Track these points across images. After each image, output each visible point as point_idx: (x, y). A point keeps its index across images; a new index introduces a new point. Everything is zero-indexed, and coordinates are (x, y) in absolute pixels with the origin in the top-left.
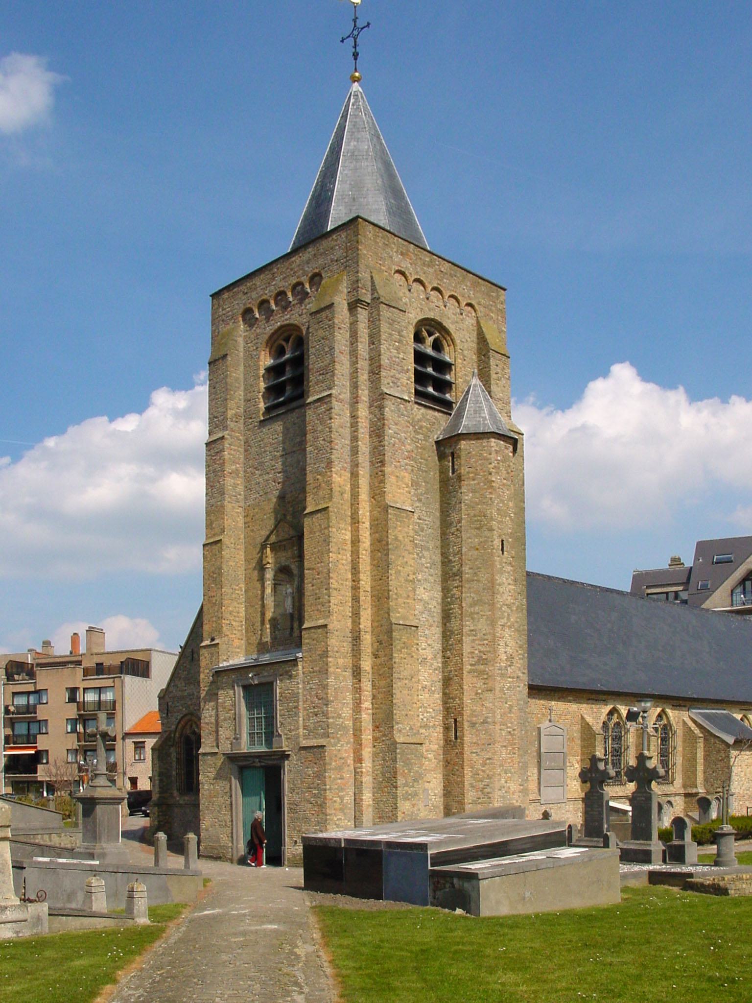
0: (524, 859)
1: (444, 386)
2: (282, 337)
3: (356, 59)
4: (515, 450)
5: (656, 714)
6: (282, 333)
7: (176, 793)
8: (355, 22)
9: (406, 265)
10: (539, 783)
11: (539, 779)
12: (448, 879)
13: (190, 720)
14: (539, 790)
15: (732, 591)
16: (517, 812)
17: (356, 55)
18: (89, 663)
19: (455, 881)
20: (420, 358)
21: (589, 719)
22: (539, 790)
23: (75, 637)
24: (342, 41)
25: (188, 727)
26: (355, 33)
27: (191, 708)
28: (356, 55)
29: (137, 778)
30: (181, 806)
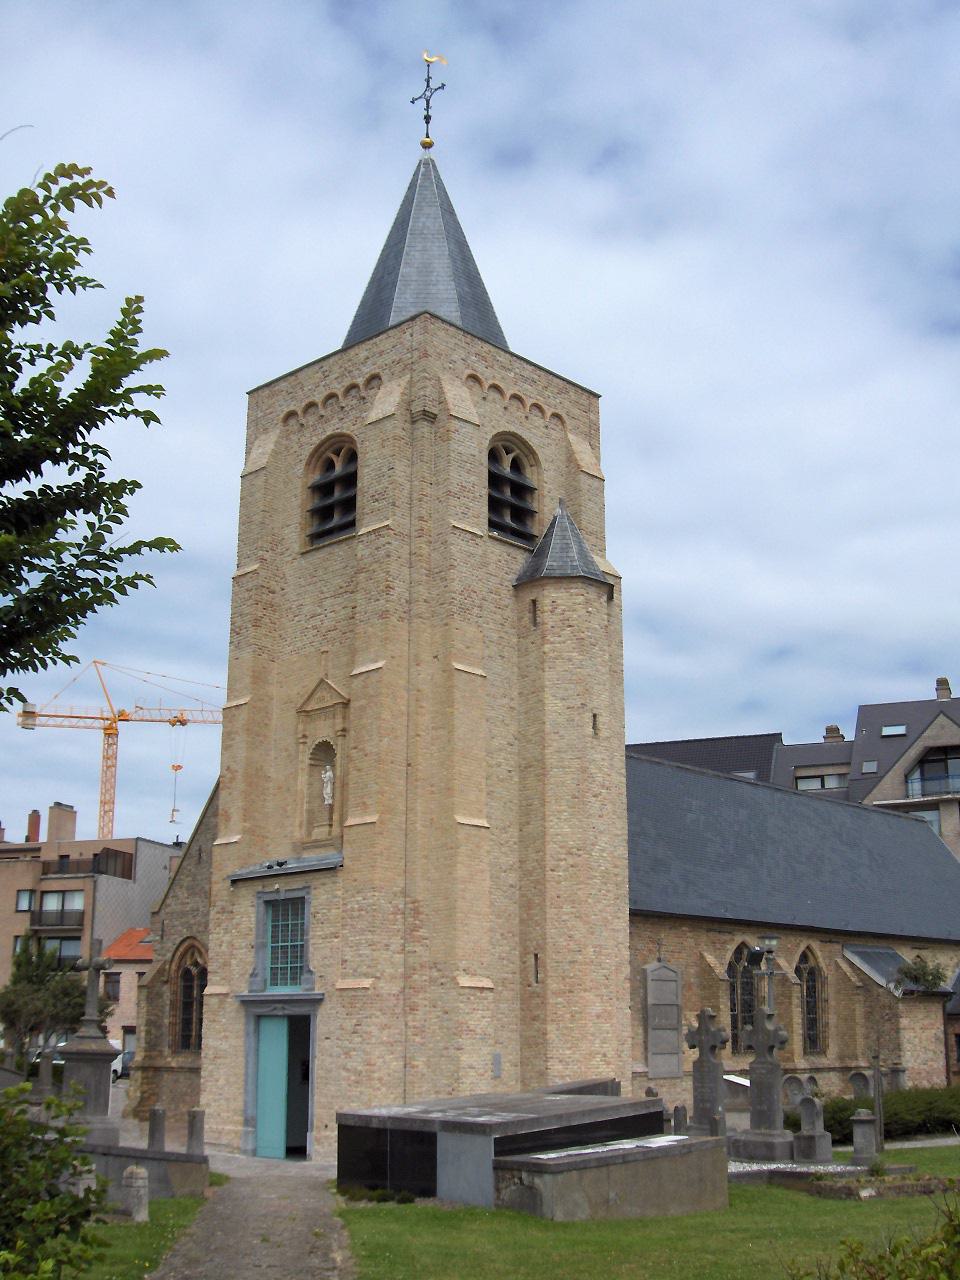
0: (610, 1148)
1: (522, 514)
2: (332, 449)
3: (427, 123)
4: (610, 598)
5: (800, 952)
6: (331, 446)
7: (167, 1051)
8: (428, 82)
9: (481, 370)
10: (646, 1049)
11: (645, 1042)
12: (515, 1173)
13: (193, 946)
14: (646, 1059)
15: (906, 777)
16: (610, 1087)
17: (428, 119)
18: (50, 855)
19: (524, 1175)
20: (495, 480)
21: (710, 959)
22: (646, 1059)
23: (35, 818)
24: (413, 102)
25: (189, 956)
26: (428, 94)
27: (195, 928)
28: (428, 119)
29: (123, 1027)
30: (171, 1070)
